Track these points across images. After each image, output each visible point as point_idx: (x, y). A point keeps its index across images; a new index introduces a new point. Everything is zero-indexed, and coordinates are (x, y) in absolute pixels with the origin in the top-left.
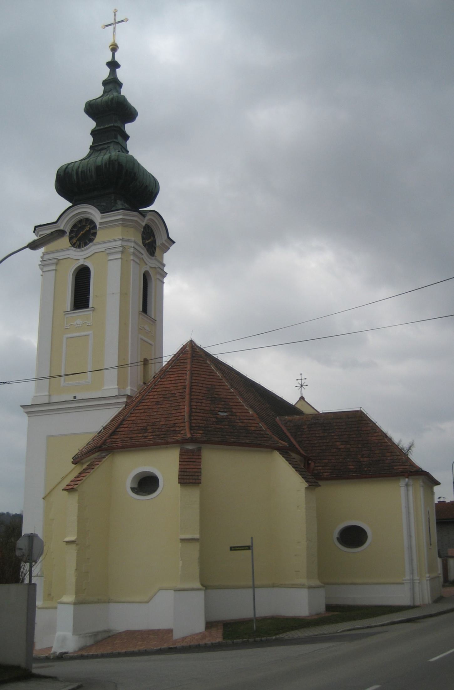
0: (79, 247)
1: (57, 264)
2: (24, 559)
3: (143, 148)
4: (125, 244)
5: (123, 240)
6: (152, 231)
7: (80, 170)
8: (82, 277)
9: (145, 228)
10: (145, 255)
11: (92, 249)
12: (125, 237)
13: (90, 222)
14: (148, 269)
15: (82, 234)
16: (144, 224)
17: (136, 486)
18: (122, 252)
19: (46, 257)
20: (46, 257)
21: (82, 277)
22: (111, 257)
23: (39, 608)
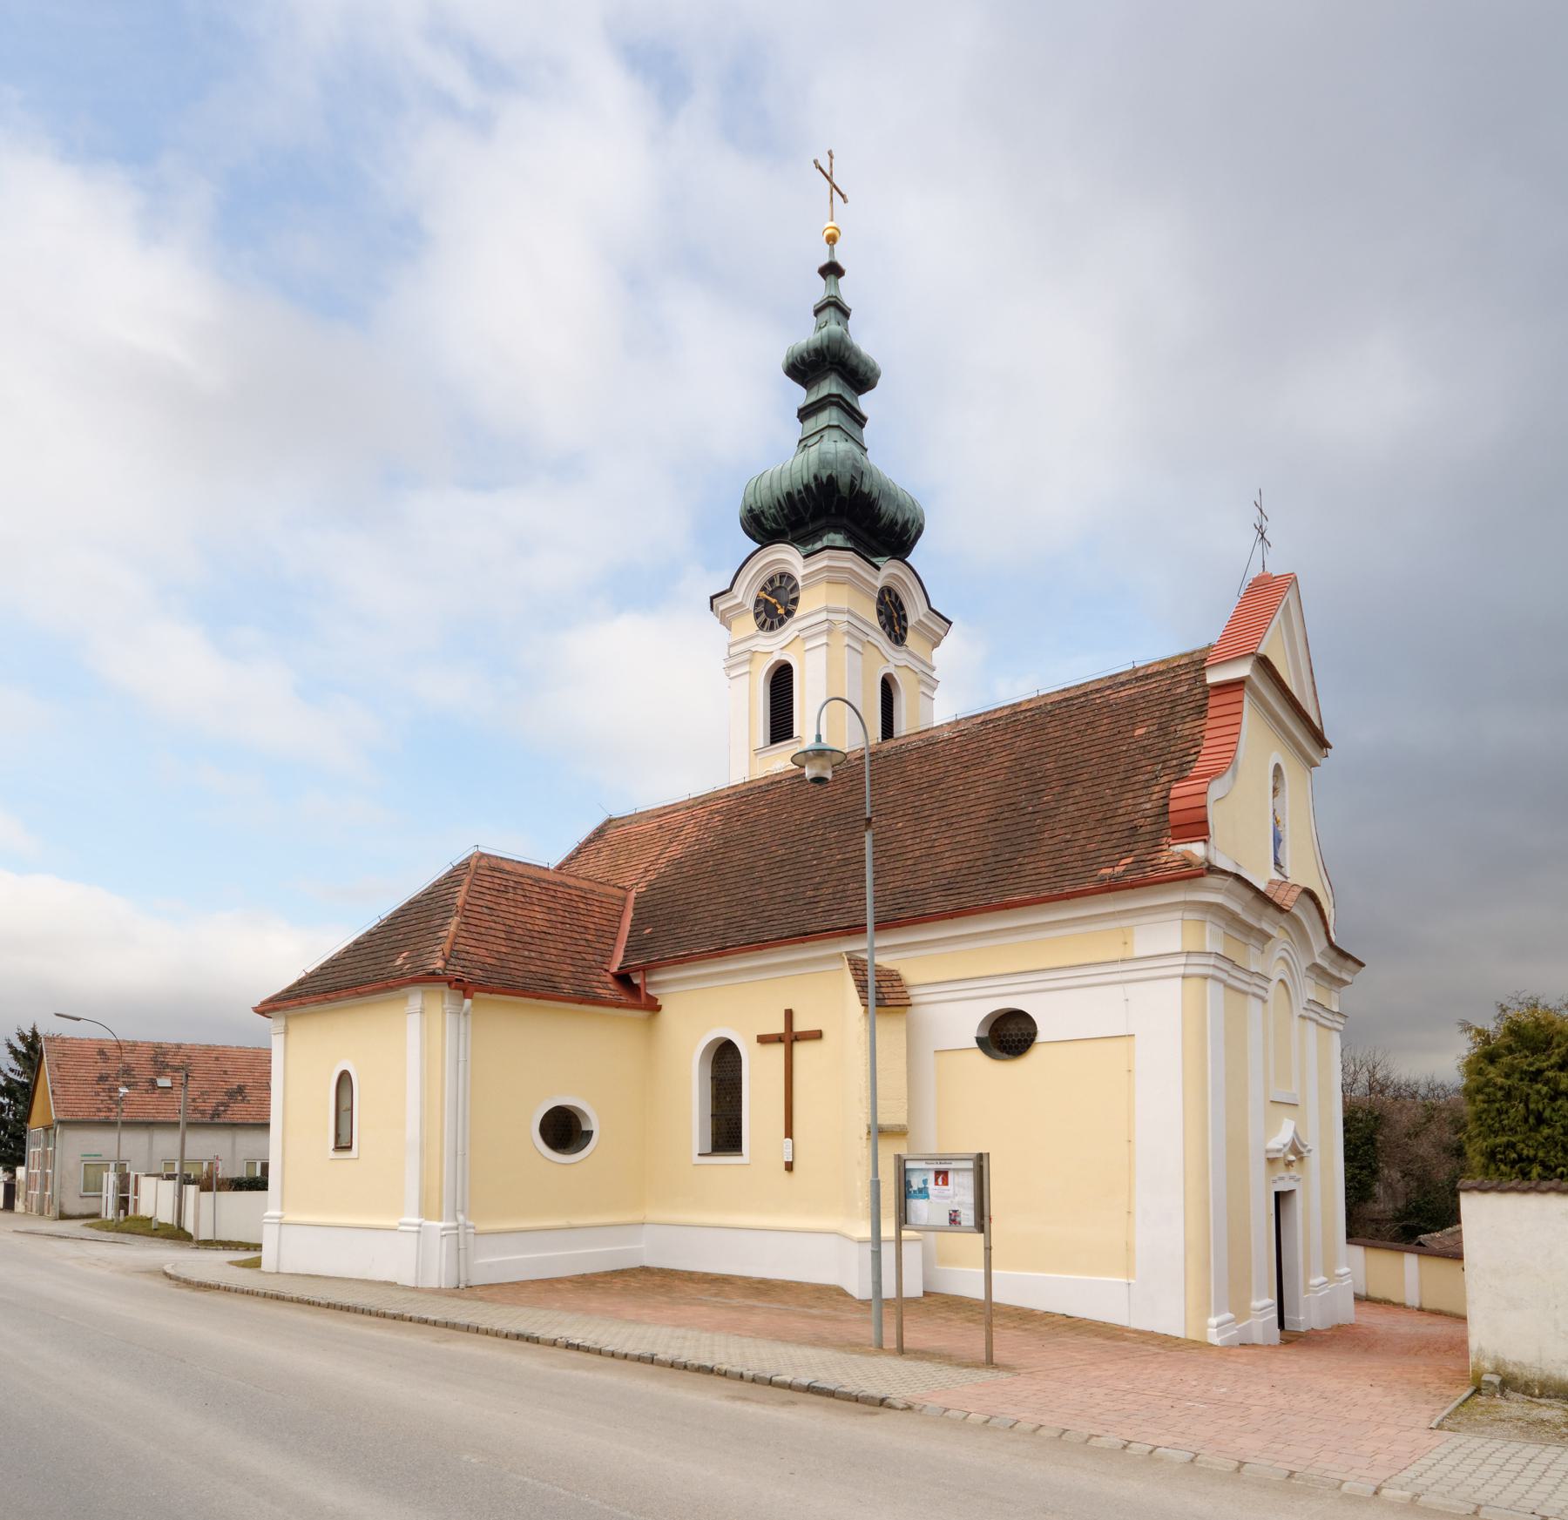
0: (772, 628)
1: (750, 661)
2: (1442, 1175)
3: (898, 447)
4: (832, 617)
5: (828, 610)
6: (897, 597)
7: (775, 485)
8: (781, 680)
9: (882, 591)
10: (881, 639)
11: (791, 629)
12: (832, 605)
13: (786, 577)
14: (891, 670)
15: (776, 605)
16: (879, 584)
17: (985, 1034)
18: (829, 632)
19: (734, 650)
20: (734, 650)
21: (781, 680)
22: (809, 645)
23: (234, 1144)
